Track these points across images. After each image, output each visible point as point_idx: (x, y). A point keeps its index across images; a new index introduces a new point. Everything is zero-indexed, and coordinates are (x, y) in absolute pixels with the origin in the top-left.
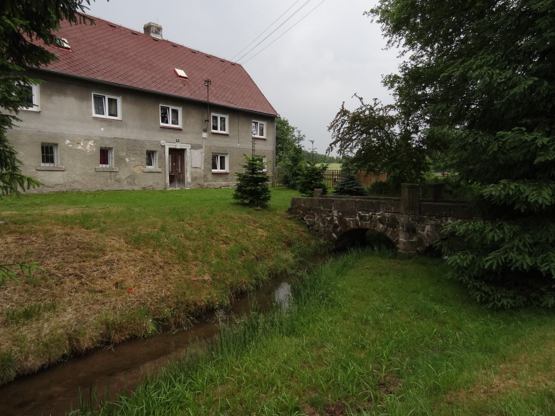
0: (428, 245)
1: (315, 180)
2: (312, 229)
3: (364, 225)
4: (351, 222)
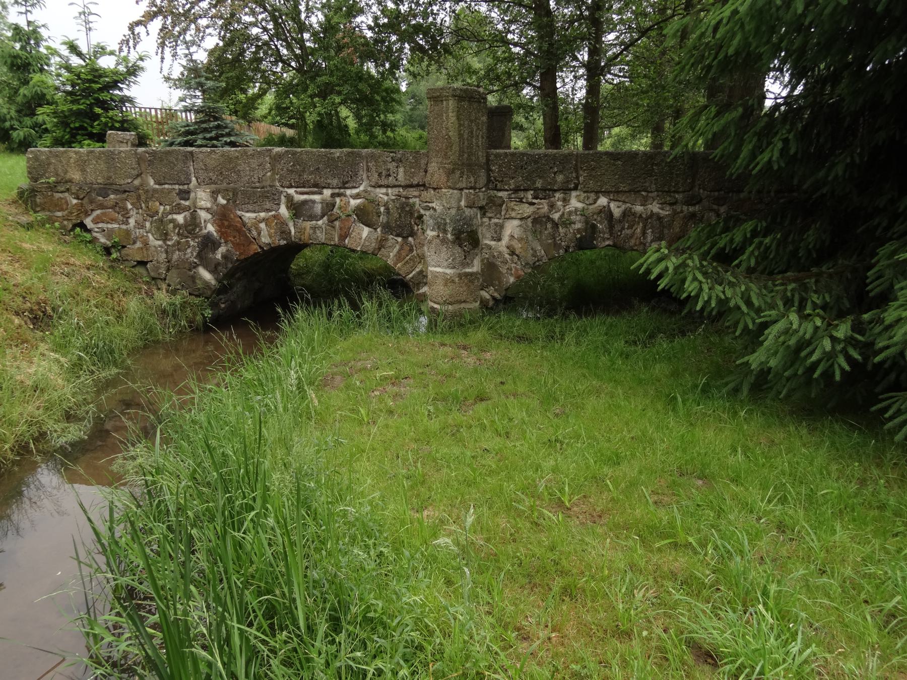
0: (512, 280)
3: (308, 231)
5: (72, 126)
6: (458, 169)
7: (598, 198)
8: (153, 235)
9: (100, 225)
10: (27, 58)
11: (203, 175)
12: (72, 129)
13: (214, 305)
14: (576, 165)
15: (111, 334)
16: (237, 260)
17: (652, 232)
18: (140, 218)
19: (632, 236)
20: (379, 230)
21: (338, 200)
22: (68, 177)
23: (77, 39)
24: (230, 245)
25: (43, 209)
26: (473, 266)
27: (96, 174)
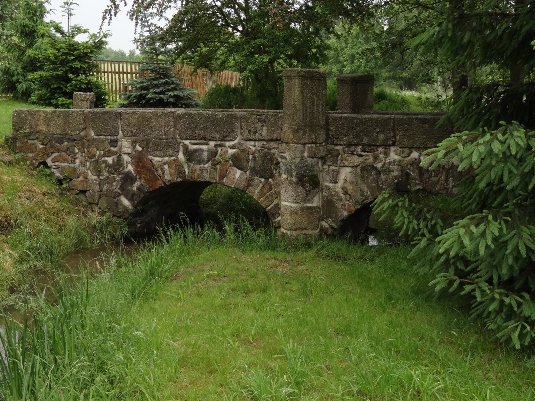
0: (345, 214)
1: (75, 71)
2: (69, 189)
3: (198, 172)
4: (166, 167)
5: (52, 87)
6: (301, 129)
7: (411, 152)
8: (91, 171)
9: (57, 164)
10: (33, 27)
11: (127, 129)
12: (52, 89)
13: (129, 225)
14: (394, 127)
15: (52, 241)
16: (148, 192)
17: (453, 180)
18: (83, 159)
19: (437, 183)
20: (247, 172)
21: (219, 149)
22: (38, 129)
23: (61, 23)
24: (143, 180)
25: (20, 152)
26: (313, 202)
27: (56, 129)
